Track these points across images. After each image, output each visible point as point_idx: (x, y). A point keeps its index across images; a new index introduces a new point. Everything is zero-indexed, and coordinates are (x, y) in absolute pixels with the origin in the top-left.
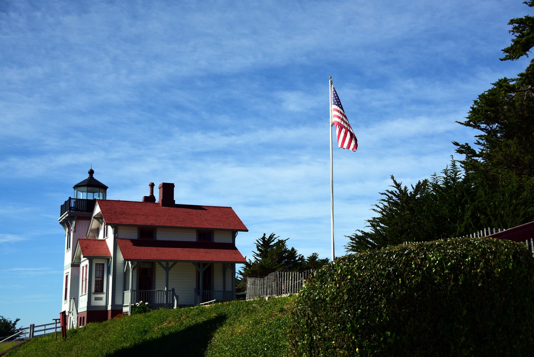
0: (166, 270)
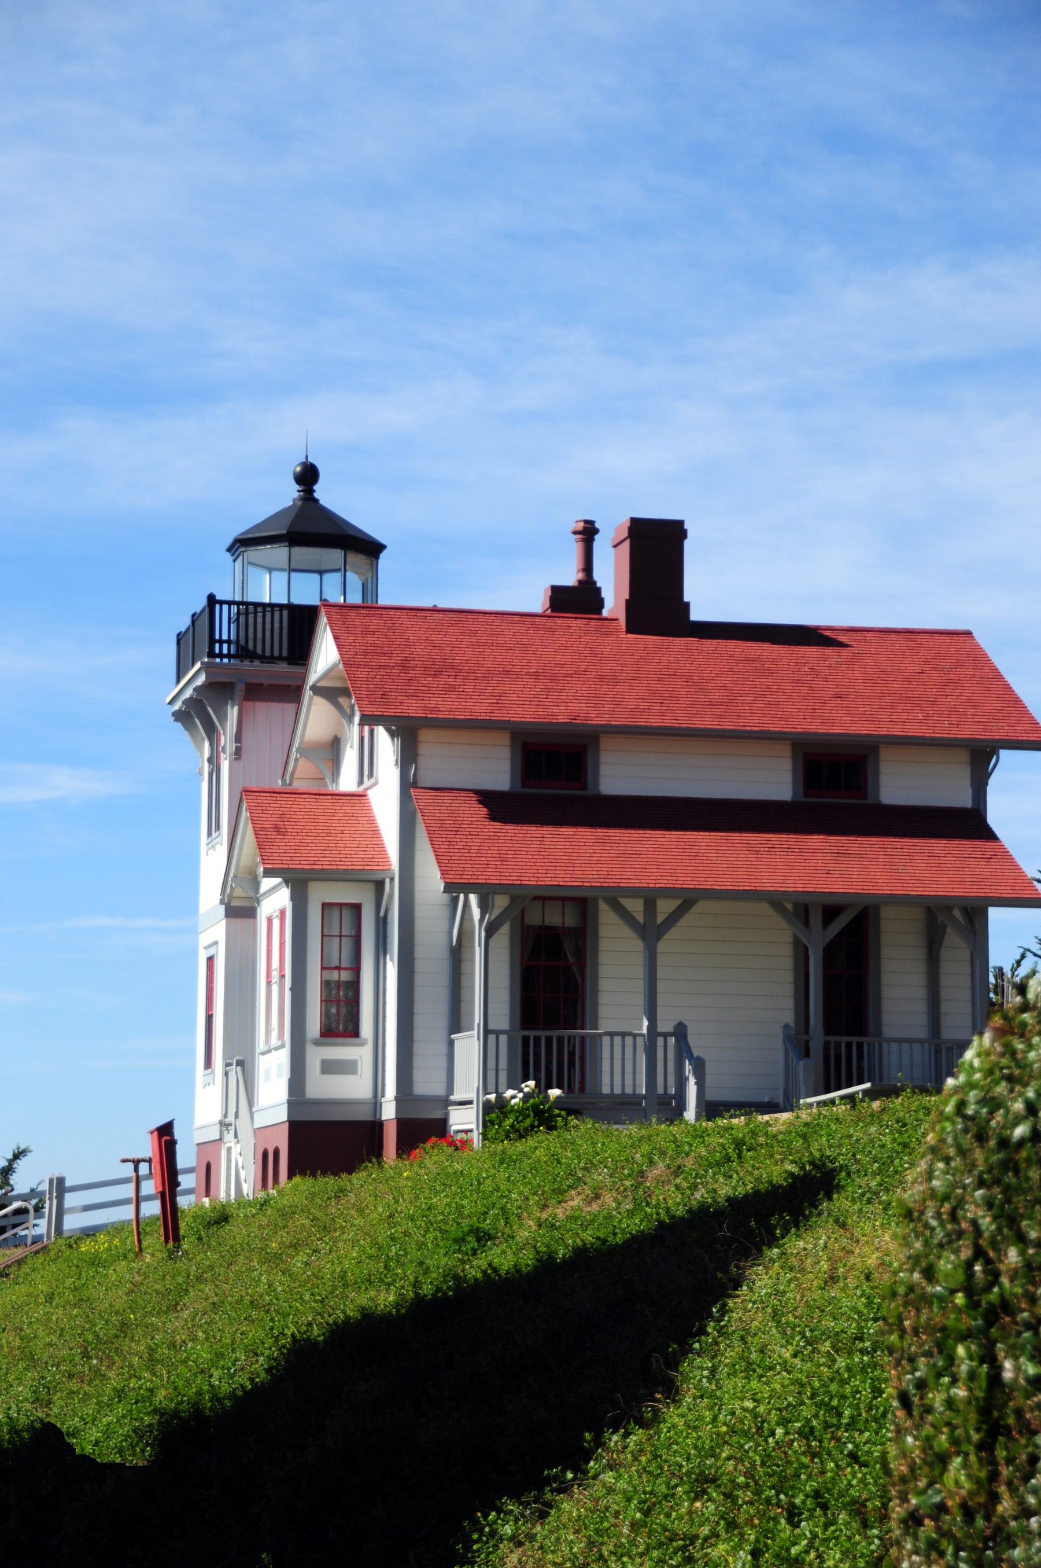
0: (643, 938)
